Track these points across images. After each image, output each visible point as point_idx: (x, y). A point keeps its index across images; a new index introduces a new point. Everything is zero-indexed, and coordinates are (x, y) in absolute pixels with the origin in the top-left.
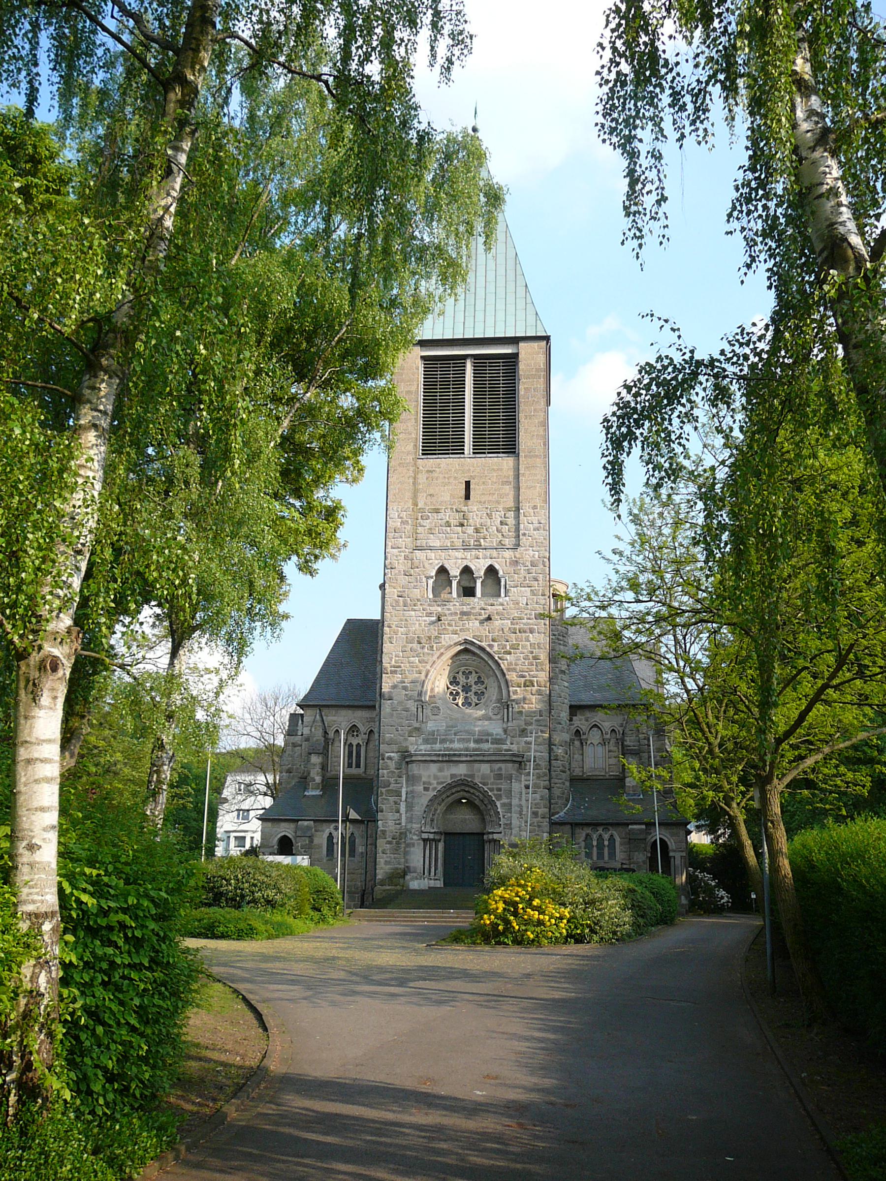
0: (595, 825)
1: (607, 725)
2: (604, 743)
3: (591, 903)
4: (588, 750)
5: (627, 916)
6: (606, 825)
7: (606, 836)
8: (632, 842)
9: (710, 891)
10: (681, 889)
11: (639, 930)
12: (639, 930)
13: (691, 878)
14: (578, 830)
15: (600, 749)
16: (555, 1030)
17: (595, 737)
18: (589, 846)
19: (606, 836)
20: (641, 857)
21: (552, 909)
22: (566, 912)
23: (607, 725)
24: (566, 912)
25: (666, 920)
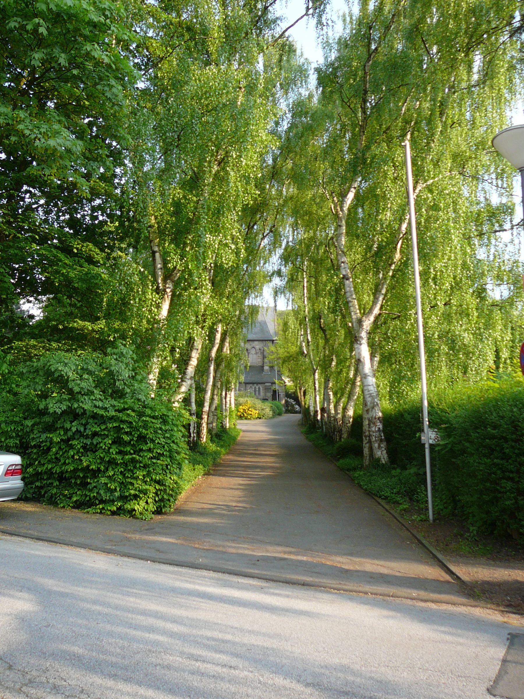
0: (253, 383)
1: (257, 347)
2: (256, 353)
3: (263, 409)
4: (250, 356)
5: (271, 413)
6: (257, 383)
7: (257, 387)
8: (267, 389)
9: (292, 406)
10: (283, 405)
11: (274, 416)
12: (274, 416)
13: (286, 402)
14: (247, 385)
15: (255, 356)
16: (276, 433)
17: (253, 351)
18: (255, 391)
19: (257, 387)
20: (269, 395)
21: (253, 411)
22: (257, 412)
23: (257, 347)
24: (257, 412)
25: (280, 414)
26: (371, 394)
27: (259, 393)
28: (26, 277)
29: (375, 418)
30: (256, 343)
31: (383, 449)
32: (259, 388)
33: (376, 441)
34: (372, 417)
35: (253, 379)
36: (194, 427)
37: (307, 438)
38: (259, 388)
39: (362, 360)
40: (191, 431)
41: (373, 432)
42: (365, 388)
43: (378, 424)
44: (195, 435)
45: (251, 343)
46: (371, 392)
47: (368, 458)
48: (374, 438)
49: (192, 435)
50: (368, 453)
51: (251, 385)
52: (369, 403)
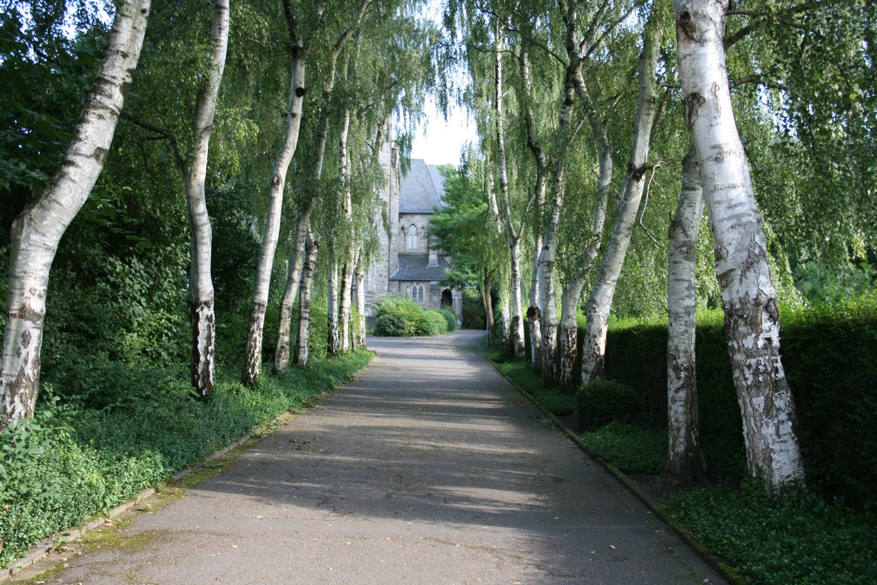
2: (418, 234)
6: (418, 281)
7: (418, 287)
14: (402, 284)
17: (413, 230)
18: (414, 293)
19: (418, 287)
26: (739, 216)
27: (421, 297)
28: (16, 66)
29: (757, 303)
30: (418, 217)
31: (783, 416)
32: (421, 289)
33: (757, 385)
34: (743, 301)
35: (412, 274)
36: (209, 338)
37: (498, 370)
38: (421, 289)
39: (707, 95)
40: (201, 347)
41: (749, 354)
42: (717, 197)
43: (766, 325)
44: (211, 358)
45: (409, 217)
46: (739, 210)
47: (683, 432)
48: (748, 374)
49: (202, 359)
50: (682, 418)
51: (408, 284)
52: (731, 249)
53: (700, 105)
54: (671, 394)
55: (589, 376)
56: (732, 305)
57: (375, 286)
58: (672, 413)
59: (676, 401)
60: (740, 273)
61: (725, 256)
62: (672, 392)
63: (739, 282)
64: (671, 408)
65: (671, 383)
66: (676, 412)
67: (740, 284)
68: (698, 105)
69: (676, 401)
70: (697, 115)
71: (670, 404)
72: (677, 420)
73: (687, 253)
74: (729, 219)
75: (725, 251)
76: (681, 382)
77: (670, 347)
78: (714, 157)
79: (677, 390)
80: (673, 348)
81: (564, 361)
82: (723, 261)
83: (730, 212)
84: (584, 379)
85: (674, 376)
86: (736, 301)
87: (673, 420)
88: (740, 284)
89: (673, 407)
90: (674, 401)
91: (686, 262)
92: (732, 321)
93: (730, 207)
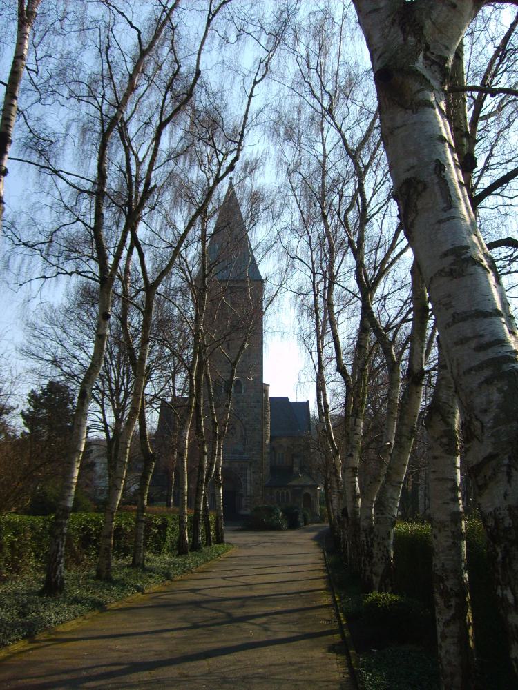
32: (287, 493)
38: (287, 493)
53: (419, 194)
54: (440, 628)
55: (379, 579)
56: (498, 522)
57: (252, 491)
58: (442, 653)
59: (446, 637)
60: (506, 462)
61: (478, 432)
62: (441, 624)
63: (505, 478)
64: (441, 646)
65: (440, 613)
66: (447, 652)
67: (509, 481)
68: (415, 197)
69: (446, 637)
70: (416, 211)
71: (439, 641)
72: (449, 663)
73: (448, 445)
74: (480, 368)
75: (477, 423)
76: (452, 612)
77: (435, 566)
78: (447, 270)
79: (447, 624)
80: (439, 566)
81: (364, 560)
82: (475, 442)
83: (483, 356)
84: (374, 582)
85: (443, 604)
86: (504, 512)
87: (445, 662)
88: (509, 481)
89: (443, 644)
90: (444, 637)
91: (448, 456)
92: (499, 550)
93: (481, 348)
